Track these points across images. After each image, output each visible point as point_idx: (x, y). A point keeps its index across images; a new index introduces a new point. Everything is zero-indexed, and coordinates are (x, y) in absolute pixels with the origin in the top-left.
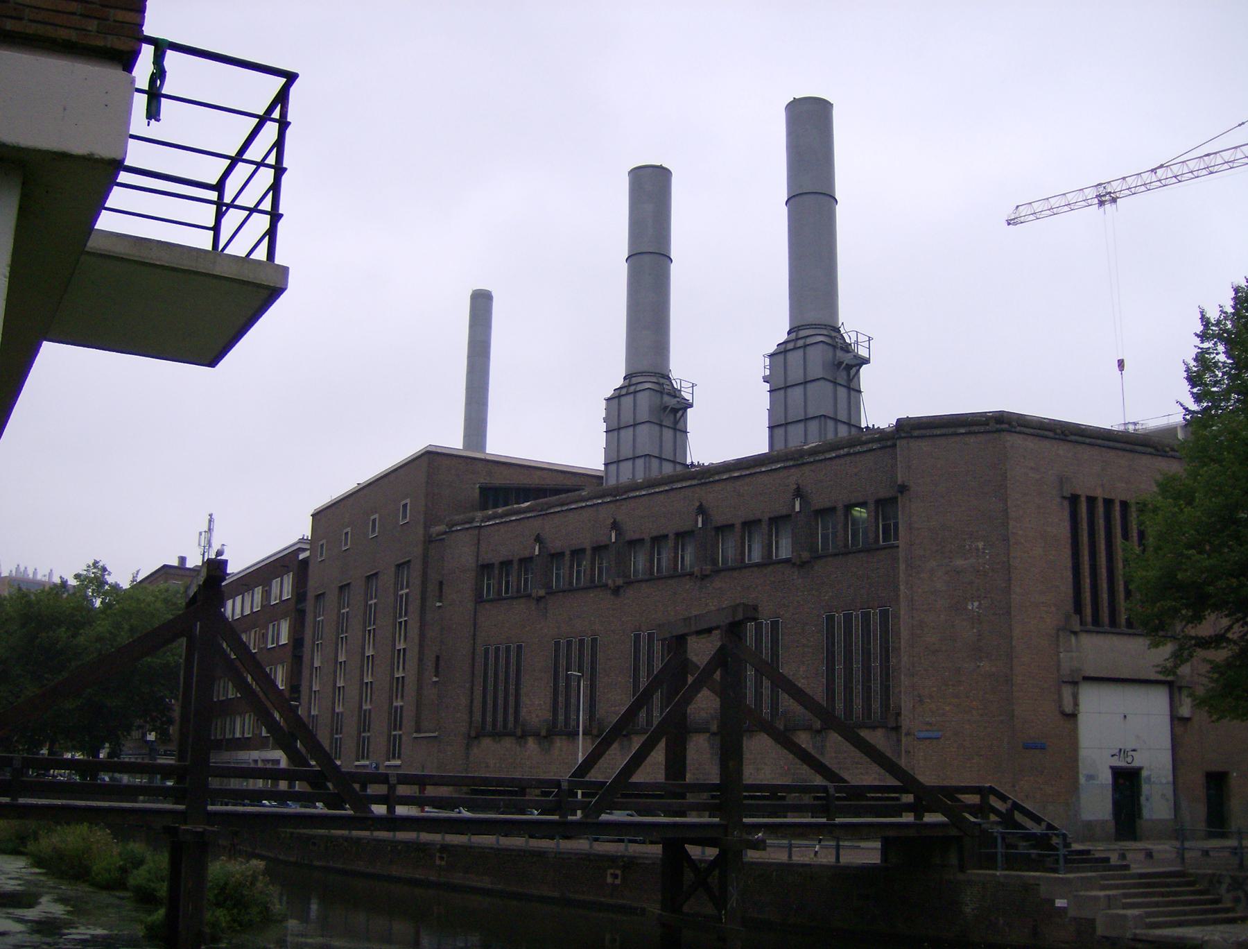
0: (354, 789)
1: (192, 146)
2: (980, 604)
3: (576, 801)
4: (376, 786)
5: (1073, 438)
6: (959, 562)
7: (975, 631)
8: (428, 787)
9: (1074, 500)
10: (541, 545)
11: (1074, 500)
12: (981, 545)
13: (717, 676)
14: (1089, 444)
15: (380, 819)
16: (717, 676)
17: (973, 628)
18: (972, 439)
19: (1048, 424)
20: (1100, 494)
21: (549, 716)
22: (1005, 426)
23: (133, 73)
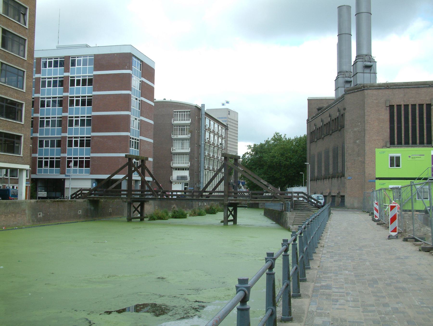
0: (93, 192)
1: (135, 55)
2: (359, 141)
3: (263, 196)
4: (196, 193)
5: (392, 87)
6: (355, 129)
7: (358, 149)
8: (299, 194)
9: (391, 107)
10: (339, 112)
11: (391, 107)
12: (359, 124)
13: (223, 170)
14: (398, 88)
15: (171, 199)
16: (223, 170)
17: (358, 148)
18: (358, 93)
19: (382, 85)
20: (402, 103)
21: (342, 170)
22: (366, 88)
23: (94, 72)
